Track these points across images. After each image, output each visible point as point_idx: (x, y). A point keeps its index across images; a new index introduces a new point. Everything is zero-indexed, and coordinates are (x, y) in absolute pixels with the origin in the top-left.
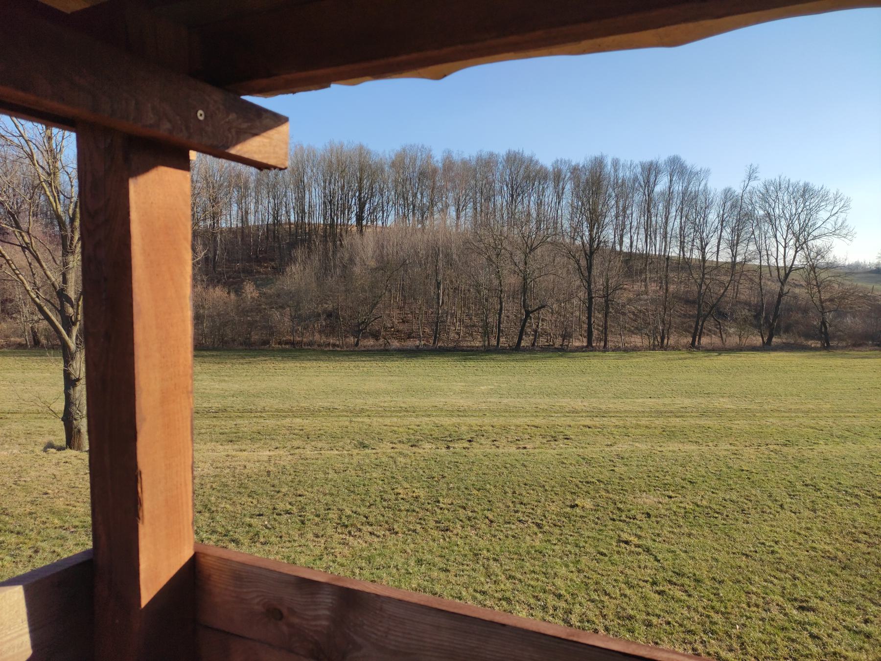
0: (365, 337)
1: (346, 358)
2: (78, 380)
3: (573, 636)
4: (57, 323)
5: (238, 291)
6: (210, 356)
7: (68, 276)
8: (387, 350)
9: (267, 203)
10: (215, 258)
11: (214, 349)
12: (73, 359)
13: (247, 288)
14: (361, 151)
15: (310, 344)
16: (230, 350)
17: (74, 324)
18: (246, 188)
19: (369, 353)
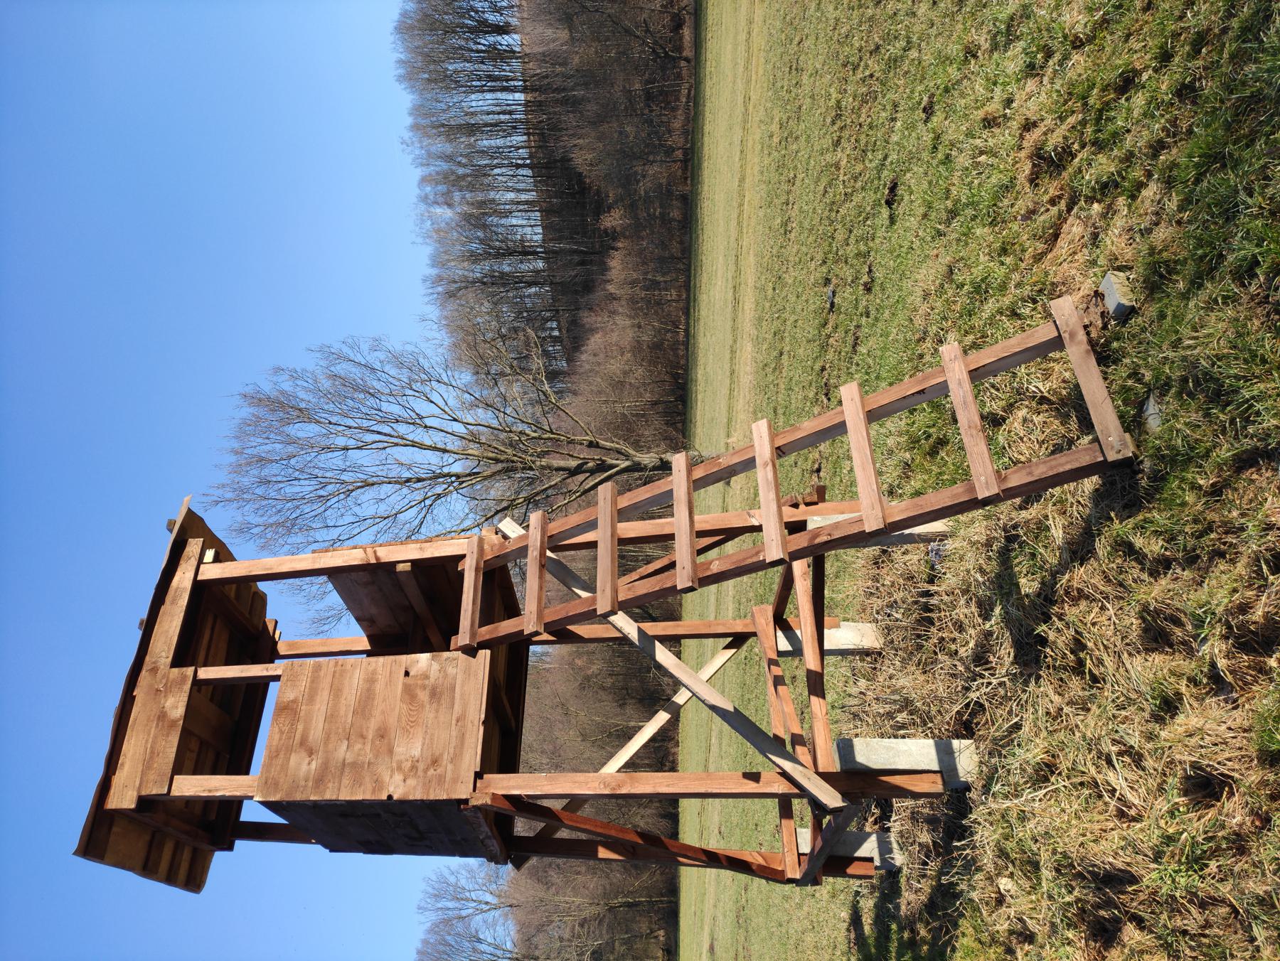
0: (680, 49)
1: (702, 85)
2: (661, 459)
3: (217, 790)
4: (602, 477)
5: (613, 235)
6: (695, 279)
7: (556, 465)
8: (696, 10)
9: (501, 174)
10: (582, 252)
11: (689, 270)
12: (639, 464)
13: (609, 225)
14: (404, 28)
15: (686, 133)
16: (690, 246)
17: (604, 461)
18: (482, 204)
19: (698, 43)
